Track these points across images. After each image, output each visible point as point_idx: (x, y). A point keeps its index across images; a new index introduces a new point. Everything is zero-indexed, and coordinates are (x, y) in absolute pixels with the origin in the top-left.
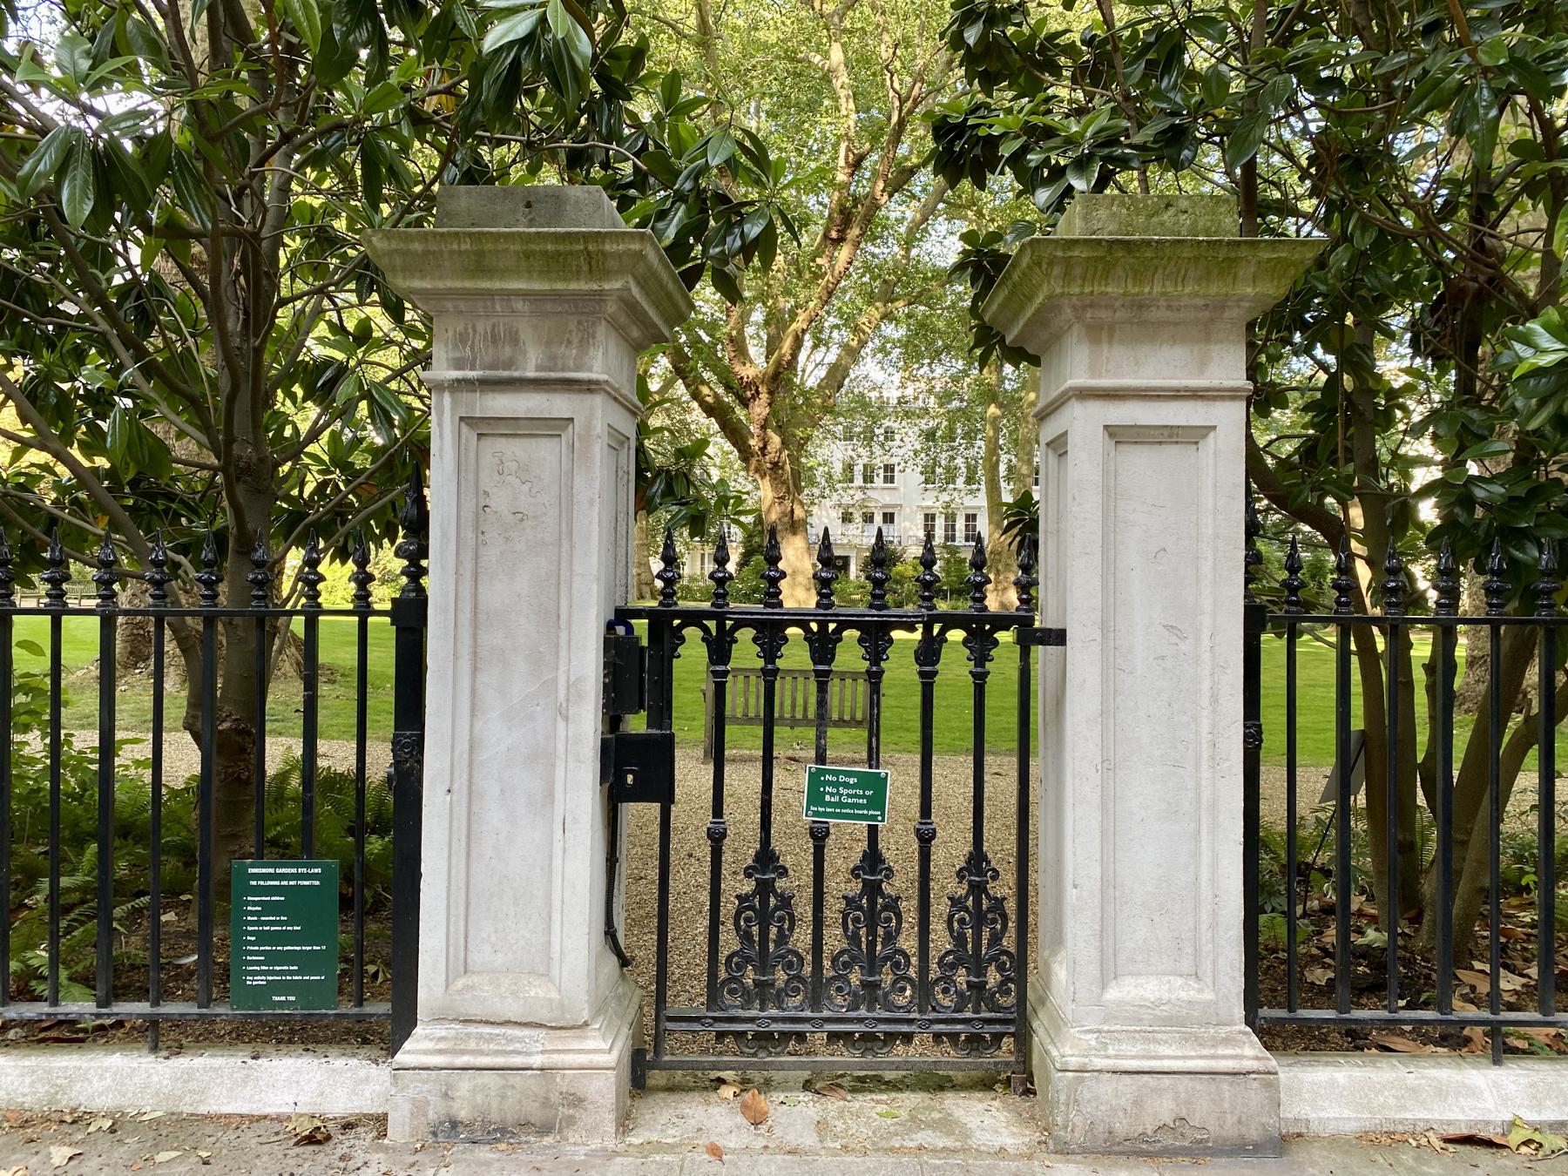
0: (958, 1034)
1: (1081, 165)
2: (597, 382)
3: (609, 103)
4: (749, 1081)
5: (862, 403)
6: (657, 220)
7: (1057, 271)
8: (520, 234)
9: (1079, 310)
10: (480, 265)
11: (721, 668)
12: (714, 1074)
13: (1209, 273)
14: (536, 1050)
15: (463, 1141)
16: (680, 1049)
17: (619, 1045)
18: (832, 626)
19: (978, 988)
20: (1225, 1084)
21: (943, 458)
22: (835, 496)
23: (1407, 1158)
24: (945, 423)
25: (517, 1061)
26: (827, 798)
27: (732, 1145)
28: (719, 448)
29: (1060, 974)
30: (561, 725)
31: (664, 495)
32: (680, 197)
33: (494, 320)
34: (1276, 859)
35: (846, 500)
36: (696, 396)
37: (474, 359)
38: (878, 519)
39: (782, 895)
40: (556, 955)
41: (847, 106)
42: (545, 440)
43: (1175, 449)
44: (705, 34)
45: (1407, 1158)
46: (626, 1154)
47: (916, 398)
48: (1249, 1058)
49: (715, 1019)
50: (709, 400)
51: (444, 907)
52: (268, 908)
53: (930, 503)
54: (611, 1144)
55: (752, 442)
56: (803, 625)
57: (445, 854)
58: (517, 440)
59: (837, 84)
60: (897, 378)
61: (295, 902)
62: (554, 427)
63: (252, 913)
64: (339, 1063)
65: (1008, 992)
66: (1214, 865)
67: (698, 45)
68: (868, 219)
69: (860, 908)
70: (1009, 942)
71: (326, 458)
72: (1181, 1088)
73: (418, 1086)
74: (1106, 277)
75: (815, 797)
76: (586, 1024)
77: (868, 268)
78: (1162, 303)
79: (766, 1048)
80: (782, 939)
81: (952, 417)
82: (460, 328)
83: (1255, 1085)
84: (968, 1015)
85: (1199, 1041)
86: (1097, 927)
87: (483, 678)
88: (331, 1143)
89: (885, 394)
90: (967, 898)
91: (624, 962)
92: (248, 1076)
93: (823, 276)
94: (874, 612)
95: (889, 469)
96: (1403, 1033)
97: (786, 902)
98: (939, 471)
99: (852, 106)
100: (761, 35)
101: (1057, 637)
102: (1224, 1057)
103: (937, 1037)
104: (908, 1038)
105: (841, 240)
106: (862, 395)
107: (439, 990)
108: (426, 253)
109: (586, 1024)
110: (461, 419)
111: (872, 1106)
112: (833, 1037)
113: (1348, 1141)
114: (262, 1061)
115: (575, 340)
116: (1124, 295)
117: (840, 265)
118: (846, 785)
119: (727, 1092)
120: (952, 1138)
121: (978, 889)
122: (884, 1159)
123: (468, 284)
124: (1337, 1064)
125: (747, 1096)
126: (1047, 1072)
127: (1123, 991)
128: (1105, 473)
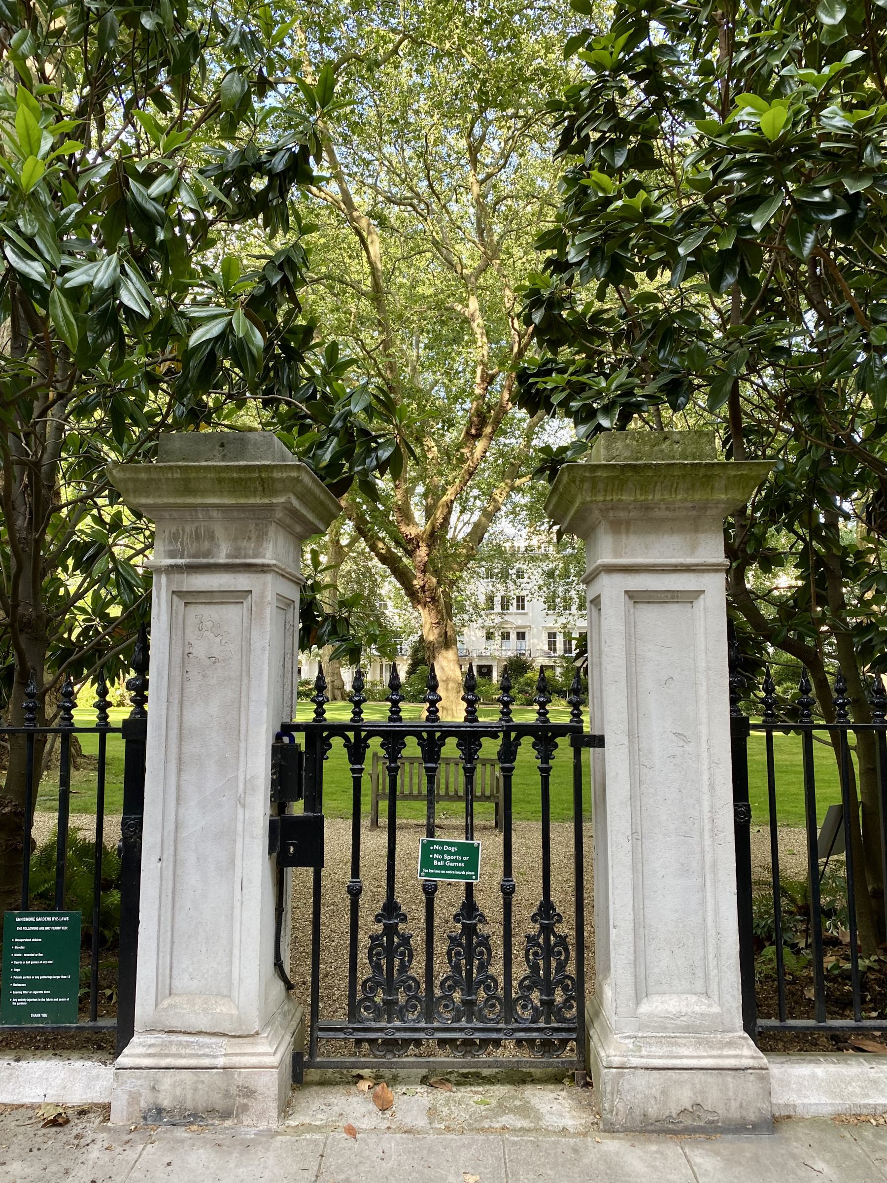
0: (534, 1040)
1: (607, 410)
2: (268, 566)
3: (289, 362)
4: (381, 1077)
5: (499, 551)
6: (317, 449)
7: (586, 485)
8: (214, 467)
9: (604, 512)
10: (187, 486)
11: (359, 766)
12: (355, 1072)
13: (693, 485)
14: (221, 1053)
15: (166, 1124)
16: (334, 1051)
17: (282, 1049)
18: (438, 734)
19: (548, 1004)
20: (729, 1077)
21: (560, 591)
22: (480, 621)
23: (868, 1134)
24: (561, 565)
25: (206, 1062)
26: (435, 862)
27: (364, 1126)
28: (389, 587)
29: (608, 993)
30: (240, 811)
31: (330, 634)
32: (334, 432)
33: (196, 524)
34: (793, 900)
35: (488, 623)
36: (373, 548)
37: (183, 551)
38: (513, 636)
39: (403, 935)
40: (235, 982)
41: (482, 340)
42: (231, 606)
43: (675, 607)
44: (377, 292)
45: (868, 1134)
46: (285, 1133)
47: (539, 547)
48: (746, 1057)
49: (354, 1029)
50: (383, 552)
51: (155, 946)
52: (30, 947)
53: (551, 625)
54: (274, 1125)
55: (415, 582)
56: (418, 735)
57: (157, 907)
58: (212, 606)
59: (474, 325)
60: (524, 532)
61: (49, 943)
62: (238, 596)
63: (18, 951)
64: (78, 1064)
65: (571, 1007)
66: (716, 911)
67: (372, 300)
68: (497, 422)
69: (460, 945)
70: (571, 968)
71: (90, 611)
72: (697, 1081)
73: (136, 1082)
74: (621, 489)
75: (427, 862)
76: (257, 1033)
77: (502, 455)
78: (663, 506)
79: (392, 1051)
80: (404, 968)
81: (567, 561)
82: (174, 530)
83: (752, 1078)
84: (542, 1025)
85: (710, 1044)
86: (632, 958)
87: (184, 776)
88: (69, 1126)
89: (516, 544)
90: (539, 936)
91: (289, 986)
92: (11, 1075)
93: (465, 462)
94: (468, 724)
95: (520, 599)
96: (874, 1038)
97: (406, 940)
98: (558, 600)
99: (485, 340)
100: (420, 290)
101: (598, 741)
102: (728, 1057)
103: (519, 1042)
104: (497, 1043)
105: (478, 436)
106: (499, 546)
107: (150, 1009)
108: (150, 480)
109: (257, 1033)
110: (173, 592)
111: (471, 1098)
112: (442, 1042)
113: (825, 1121)
114: (23, 1063)
115: (254, 537)
116: (635, 501)
117: (478, 453)
118: (449, 853)
119: (364, 1085)
120: (528, 1121)
121: (547, 930)
122: (476, 1137)
123: (179, 501)
124: (818, 1062)
125: (378, 1088)
126: (598, 1069)
127: (652, 1006)
128: (627, 623)
